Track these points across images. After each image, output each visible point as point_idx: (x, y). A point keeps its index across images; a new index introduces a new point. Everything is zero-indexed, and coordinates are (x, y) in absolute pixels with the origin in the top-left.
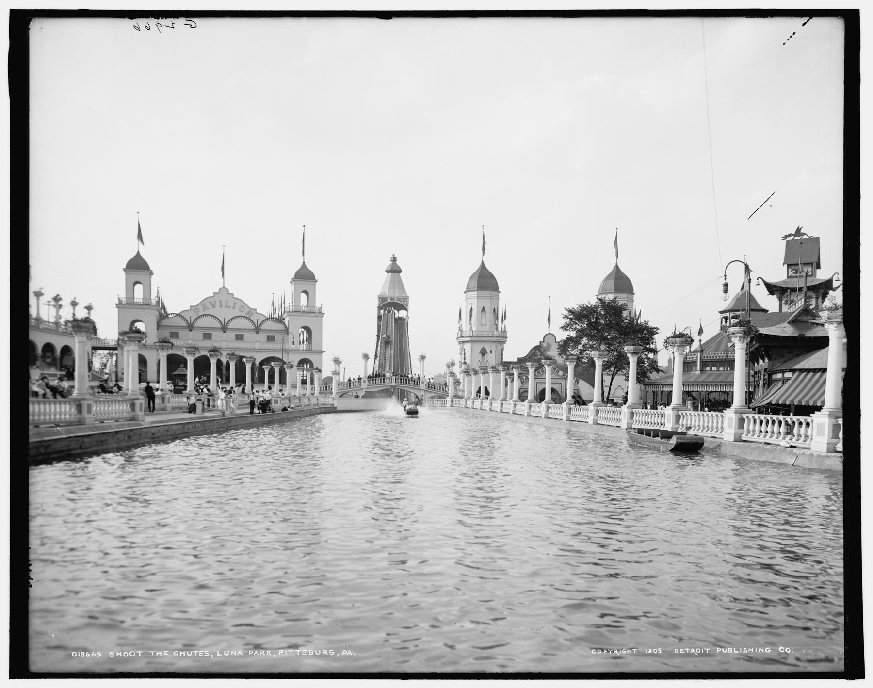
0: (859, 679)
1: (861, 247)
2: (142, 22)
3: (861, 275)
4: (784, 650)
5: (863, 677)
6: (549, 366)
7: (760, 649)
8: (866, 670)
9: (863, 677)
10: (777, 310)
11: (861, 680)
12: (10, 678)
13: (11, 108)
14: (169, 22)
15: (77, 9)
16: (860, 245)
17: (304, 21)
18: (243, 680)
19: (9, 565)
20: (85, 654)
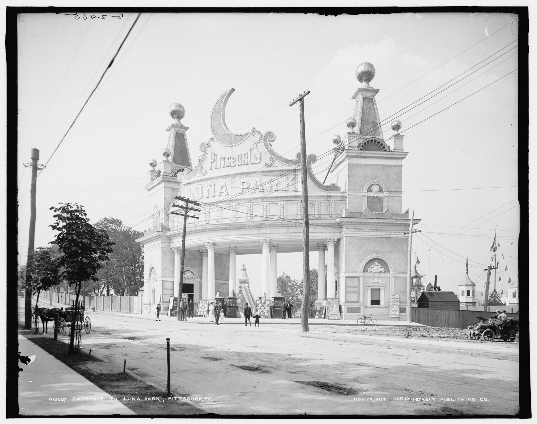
0: (528, 418)
1: (529, 153)
2: (81, 15)
3: (529, 170)
4: (483, 399)
5: (530, 417)
6: (81, 336)
7: (469, 399)
8: (532, 413)
9: (530, 417)
10: (123, 371)
11: (529, 419)
12: (7, 418)
13: (7, 67)
14: (88, 15)
15: (48, 6)
16: (529, 151)
17: (271, 15)
18: (150, 419)
19: (6, 348)
20: (57, 399)
